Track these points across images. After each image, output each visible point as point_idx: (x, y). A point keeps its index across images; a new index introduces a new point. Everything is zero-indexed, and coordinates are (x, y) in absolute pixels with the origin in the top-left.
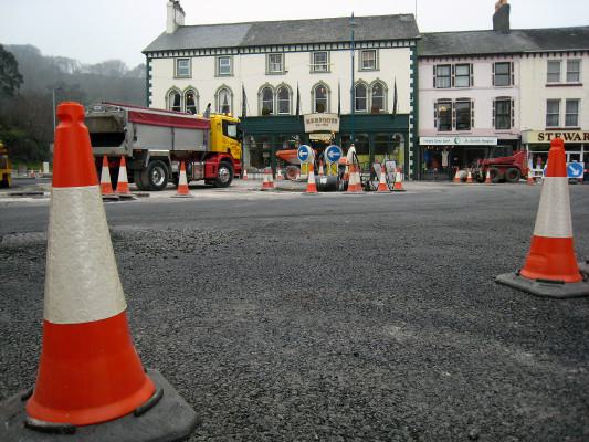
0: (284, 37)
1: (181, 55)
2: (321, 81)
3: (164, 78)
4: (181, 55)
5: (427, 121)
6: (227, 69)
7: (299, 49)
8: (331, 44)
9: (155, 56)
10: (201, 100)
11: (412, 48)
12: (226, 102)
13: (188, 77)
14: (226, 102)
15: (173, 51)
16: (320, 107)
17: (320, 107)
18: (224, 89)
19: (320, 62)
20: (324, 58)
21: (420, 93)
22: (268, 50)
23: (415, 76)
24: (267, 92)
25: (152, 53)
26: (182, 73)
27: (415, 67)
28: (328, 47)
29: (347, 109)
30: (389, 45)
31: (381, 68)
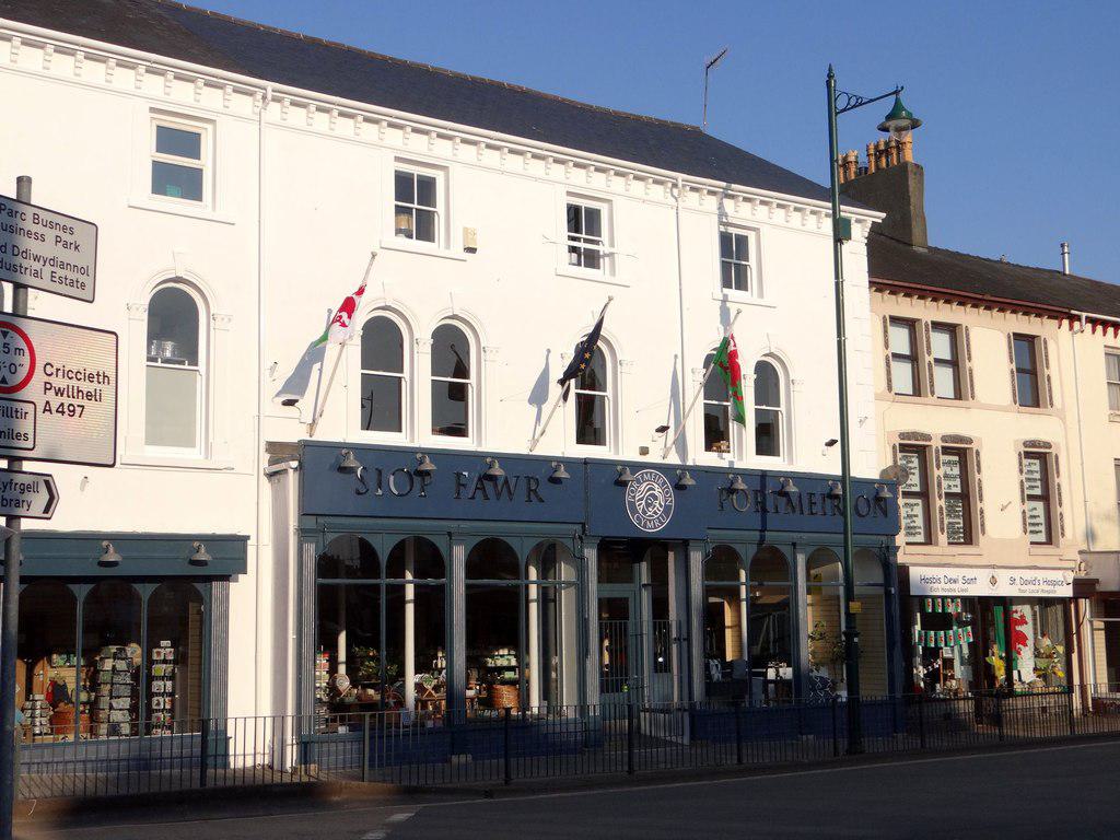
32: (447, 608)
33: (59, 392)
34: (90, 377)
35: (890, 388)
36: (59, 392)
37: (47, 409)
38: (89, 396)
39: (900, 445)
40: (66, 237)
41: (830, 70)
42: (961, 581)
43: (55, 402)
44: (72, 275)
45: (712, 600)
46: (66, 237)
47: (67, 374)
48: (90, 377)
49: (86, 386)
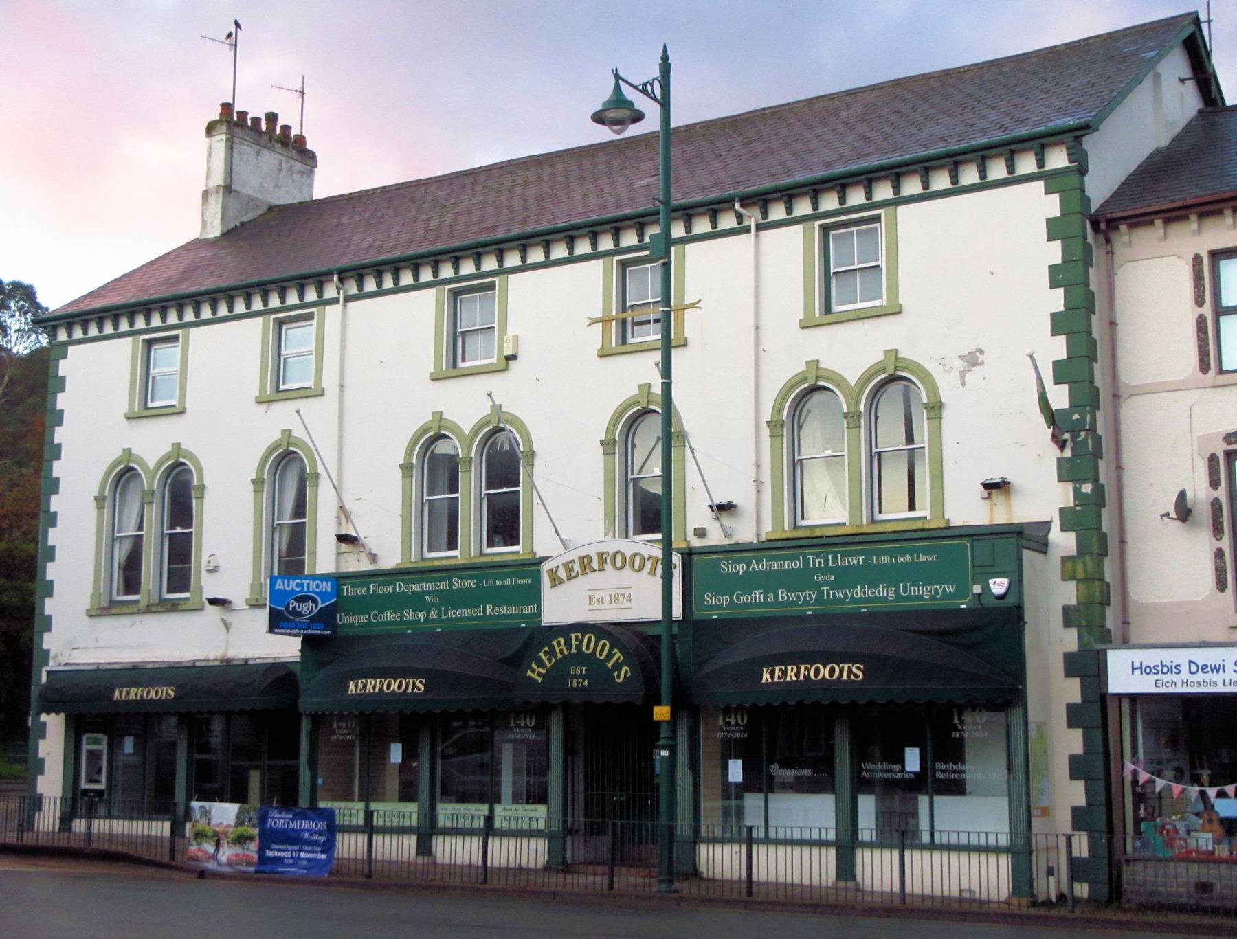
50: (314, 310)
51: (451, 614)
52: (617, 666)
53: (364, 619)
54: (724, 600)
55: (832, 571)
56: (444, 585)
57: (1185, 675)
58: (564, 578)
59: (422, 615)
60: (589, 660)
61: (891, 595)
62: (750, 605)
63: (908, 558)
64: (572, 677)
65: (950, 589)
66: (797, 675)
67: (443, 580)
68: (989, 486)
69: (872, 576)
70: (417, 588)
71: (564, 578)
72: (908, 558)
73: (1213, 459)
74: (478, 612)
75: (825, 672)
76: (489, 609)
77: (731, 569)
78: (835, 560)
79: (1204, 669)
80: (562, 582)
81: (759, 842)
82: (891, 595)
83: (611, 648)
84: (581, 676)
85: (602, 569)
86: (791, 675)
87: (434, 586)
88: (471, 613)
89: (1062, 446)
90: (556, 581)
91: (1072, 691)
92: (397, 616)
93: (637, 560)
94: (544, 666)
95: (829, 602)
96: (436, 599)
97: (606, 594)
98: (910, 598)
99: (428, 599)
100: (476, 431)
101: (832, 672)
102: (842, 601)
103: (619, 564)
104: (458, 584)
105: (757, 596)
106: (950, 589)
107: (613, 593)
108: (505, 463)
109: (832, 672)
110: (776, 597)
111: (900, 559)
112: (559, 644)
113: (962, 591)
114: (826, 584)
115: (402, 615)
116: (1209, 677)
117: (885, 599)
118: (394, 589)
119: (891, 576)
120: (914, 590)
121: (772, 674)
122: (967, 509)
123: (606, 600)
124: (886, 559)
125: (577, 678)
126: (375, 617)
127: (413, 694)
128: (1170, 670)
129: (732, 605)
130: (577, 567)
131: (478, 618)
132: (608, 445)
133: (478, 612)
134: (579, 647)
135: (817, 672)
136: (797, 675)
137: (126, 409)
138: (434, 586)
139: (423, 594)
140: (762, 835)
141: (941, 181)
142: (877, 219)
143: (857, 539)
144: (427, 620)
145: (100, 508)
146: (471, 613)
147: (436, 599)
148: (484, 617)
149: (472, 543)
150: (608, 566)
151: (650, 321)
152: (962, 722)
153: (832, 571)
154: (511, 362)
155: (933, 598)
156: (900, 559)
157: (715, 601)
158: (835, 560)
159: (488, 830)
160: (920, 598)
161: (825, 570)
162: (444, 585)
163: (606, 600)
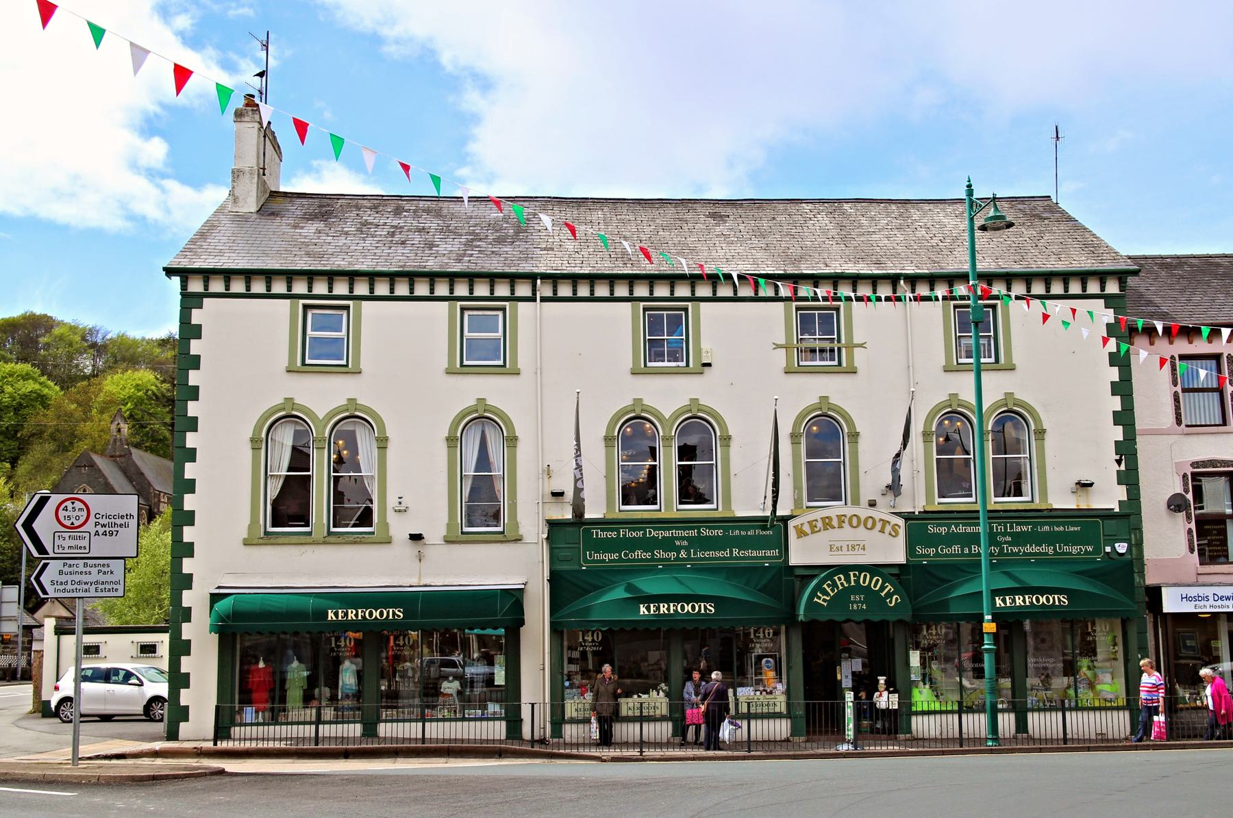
0: (1020, 251)
1: (320, 288)
2: (824, 399)
3: (247, 365)
4: (320, 288)
5: (1166, 543)
6: (331, 348)
7: (422, 289)
8: (372, 277)
9: (217, 286)
10: (863, 444)
11: (1110, 301)
12: (483, 460)
13: (344, 370)
14: (483, 460)
15: (290, 276)
16: (826, 483)
17: (826, 483)
18: (482, 418)
19: (819, 336)
20: (828, 323)
21: (1141, 443)
22: (300, 288)
23: (1123, 388)
24: (634, 432)
25: (207, 274)
26: (322, 355)
27: (1120, 361)
28: (362, 289)
29: (920, 494)
30: (602, 291)
31: (363, 366)
32: (281, 604)
33: (104, 526)
34: (122, 517)
35: (1179, 421)
36: (104, 526)
37: (97, 533)
38: (121, 525)
39: (1192, 474)
40: (106, 569)
41: (969, 186)
42: (1211, 598)
43: (101, 530)
44: (108, 587)
45: (1027, 625)
46: (106, 569)
47: (108, 517)
48: (122, 517)
49: (119, 521)
50: (507, 304)
51: (699, 555)
52: (889, 595)
53: (615, 556)
54: (932, 551)
55: (1010, 534)
56: (694, 533)
57: (1211, 602)
58: (808, 531)
59: (673, 555)
60: (858, 589)
61: (1051, 551)
62: (951, 555)
63: (1061, 528)
64: (853, 603)
65: (1090, 549)
66: (356, 615)
67: (640, 529)
68: (554, 494)
69: (1039, 539)
70: (667, 534)
71: (808, 531)
72: (1061, 528)
73: (1185, 476)
74: (727, 554)
75: (376, 614)
76: (735, 552)
77: (936, 530)
78: (1012, 527)
79: (1221, 598)
80: (806, 535)
81: (1071, 709)
82: (1051, 551)
83: (883, 583)
84: (860, 602)
85: (840, 527)
86: (351, 615)
87: (685, 534)
88: (719, 554)
89: (1119, 462)
90: (801, 533)
91: (187, 631)
92: (648, 555)
93: (870, 522)
94: (828, 594)
95: (1007, 555)
96: (685, 543)
97: (844, 545)
98: (1063, 553)
99: (678, 543)
100: (676, 415)
101: (381, 614)
102: (1017, 554)
103: (855, 524)
104: (705, 532)
105: (956, 548)
106: (1090, 549)
107: (850, 543)
108: (698, 442)
109: (381, 614)
110: (970, 550)
111: (1056, 529)
112: (840, 579)
113: (1097, 550)
114: (1006, 542)
115: (653, 554)
116: (1225, 603)
117: (1046, 554)
118: (645, 534)
119: (1051, 539)
120: (1066, 549)
121: (336, 614)
122: (1061, 499)
123: (845, 548)
124: (1047, 528)
125: (857, 604)
126: (626, 555)
127: (706, 614)
128: (1203, 599)
129: (620, 560)
130: (820, 524)
131: (725, 558)
132: (255, 442)
133: (727, 554)
134: (857, 581)
135: (371, 614)
136: (356, 615)
137: (629, 365)
138: (685, 534)
139: (673, 538)
140: (1073, 704)
141: (402, 289)
142: (347, 308)
143: (1002, 514)
144: (677, 559)
145: (255, 449)
146: (719, 554)
147: (685, 543)
148: (731, 558)
149: (668, 503)
150: (846, 525)
151: (482, 356)
152: (1094, 631)
153: (1010, 534)
154: (706, 369)
155: (1079, 554)
156: (1056, 529)
157: (925, 551)
158: (1012, 527)
159: (319, 721)
160: (1070, 554)
161: (1005, 534)
162: (694, 533)
163: (845, 548)
